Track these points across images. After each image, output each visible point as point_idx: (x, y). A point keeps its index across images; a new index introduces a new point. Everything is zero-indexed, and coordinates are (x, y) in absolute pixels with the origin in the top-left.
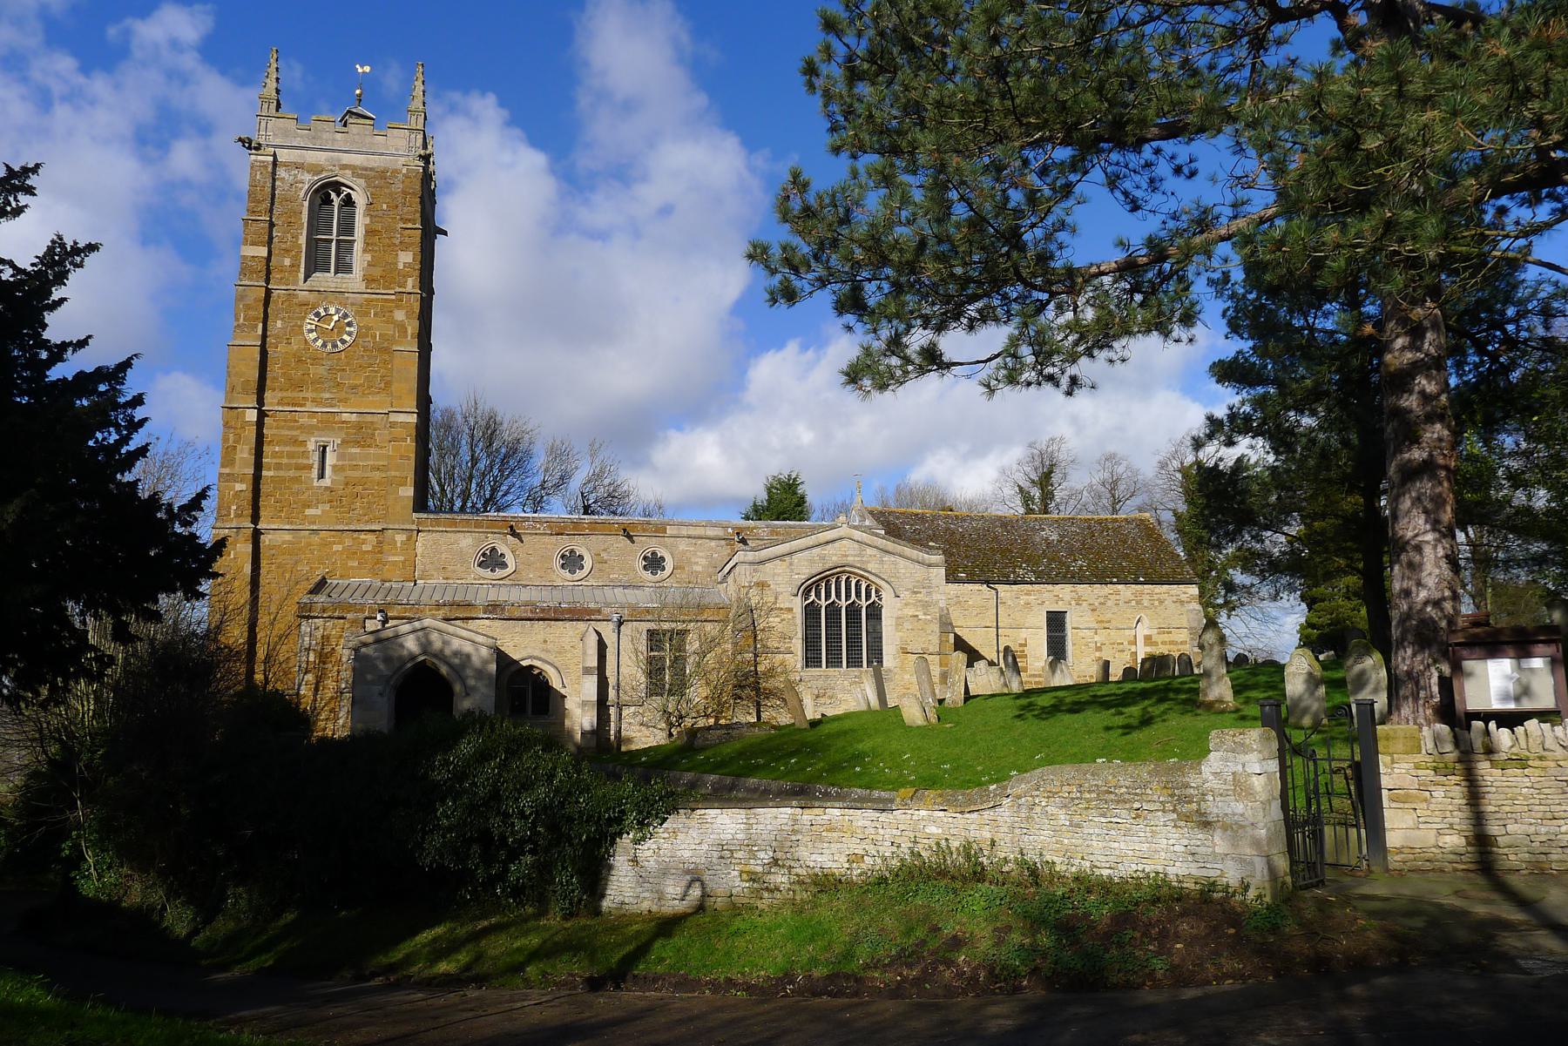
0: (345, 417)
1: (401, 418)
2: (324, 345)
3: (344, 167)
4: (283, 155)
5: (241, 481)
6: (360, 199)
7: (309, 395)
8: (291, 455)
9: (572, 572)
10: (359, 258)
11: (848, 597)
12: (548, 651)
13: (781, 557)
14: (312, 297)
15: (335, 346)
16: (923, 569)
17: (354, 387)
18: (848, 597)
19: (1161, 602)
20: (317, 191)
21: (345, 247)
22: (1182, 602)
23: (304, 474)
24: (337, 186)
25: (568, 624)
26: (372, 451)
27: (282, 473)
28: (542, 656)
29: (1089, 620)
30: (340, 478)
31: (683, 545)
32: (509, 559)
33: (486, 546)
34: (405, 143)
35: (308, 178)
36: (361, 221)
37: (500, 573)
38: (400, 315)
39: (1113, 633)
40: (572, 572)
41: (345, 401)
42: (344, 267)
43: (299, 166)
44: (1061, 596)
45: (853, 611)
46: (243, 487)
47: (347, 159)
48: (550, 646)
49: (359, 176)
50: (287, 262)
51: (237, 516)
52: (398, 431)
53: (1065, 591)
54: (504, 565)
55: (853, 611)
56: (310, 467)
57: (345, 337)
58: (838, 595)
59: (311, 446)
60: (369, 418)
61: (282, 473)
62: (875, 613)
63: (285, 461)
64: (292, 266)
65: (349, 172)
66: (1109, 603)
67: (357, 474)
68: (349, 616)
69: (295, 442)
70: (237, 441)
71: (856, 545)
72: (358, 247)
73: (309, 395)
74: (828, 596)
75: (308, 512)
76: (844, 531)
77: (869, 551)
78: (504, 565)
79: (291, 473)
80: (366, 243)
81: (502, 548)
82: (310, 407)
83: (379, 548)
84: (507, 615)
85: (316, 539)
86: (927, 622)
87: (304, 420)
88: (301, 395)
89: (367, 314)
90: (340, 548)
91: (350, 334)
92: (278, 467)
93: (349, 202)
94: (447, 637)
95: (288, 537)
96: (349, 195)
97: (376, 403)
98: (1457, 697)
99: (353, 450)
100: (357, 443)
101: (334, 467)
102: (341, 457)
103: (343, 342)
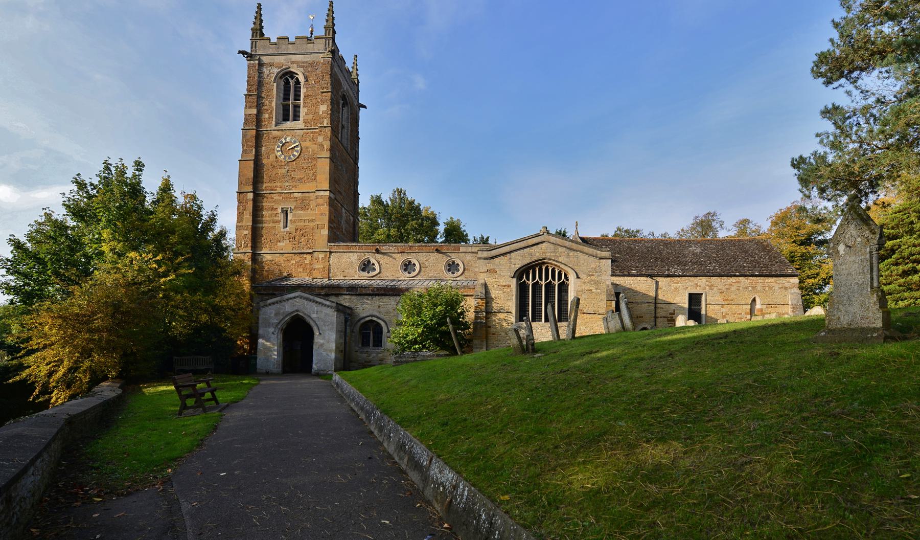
0: (296, 195)
1: (322, 193)
2: (285, 158)
3: (293, 63)
4: (265, 59)
6: (301, 78)
7: (279, 184)
10: (303, 111)
11: (547, 278)
13: (504, 254)
16: (597, 260)
18: (547, 278)
19: (770, 288)
20: (281, 78)
21: (297, 108)
22: (786, 288)
23: (276, 225)
26: (309, 212)
28: (377, 314)
29: (719, 299)
30: (294, 226)
31: (469, 257)
34: (323, 46)
35: (276, 71)
38: (320, 139)
39: (734, 307)
42: (296, 118)
43: (271, 65)
44: (699, 284)
45: (549, 286)
46: (247, 232)
48: (382, 310)
49: (301, 67)
52: (320, 201)
53: (702, 281)
54: (374, 269)
55: (549, 286)
56: (279, 221)
57: (295, 153)
58: (541, 278)
59: (280, 211)
60: (307, 195)
62: (563, 288)
65: (295, 65)
66: (733, 289)
67: (302, 224)
71: (552, 246)
73: (279, 184)
74: (534, 278)
75: (279, 244)
77: (560, 249)
79: (271, 225)
81: (373, 261)
82: (279, 190)
86: (597, 294)
90: (293, 262)
93: (298, 82)
94: (366, 308)
97: (309, 187)
102: (294, 216)
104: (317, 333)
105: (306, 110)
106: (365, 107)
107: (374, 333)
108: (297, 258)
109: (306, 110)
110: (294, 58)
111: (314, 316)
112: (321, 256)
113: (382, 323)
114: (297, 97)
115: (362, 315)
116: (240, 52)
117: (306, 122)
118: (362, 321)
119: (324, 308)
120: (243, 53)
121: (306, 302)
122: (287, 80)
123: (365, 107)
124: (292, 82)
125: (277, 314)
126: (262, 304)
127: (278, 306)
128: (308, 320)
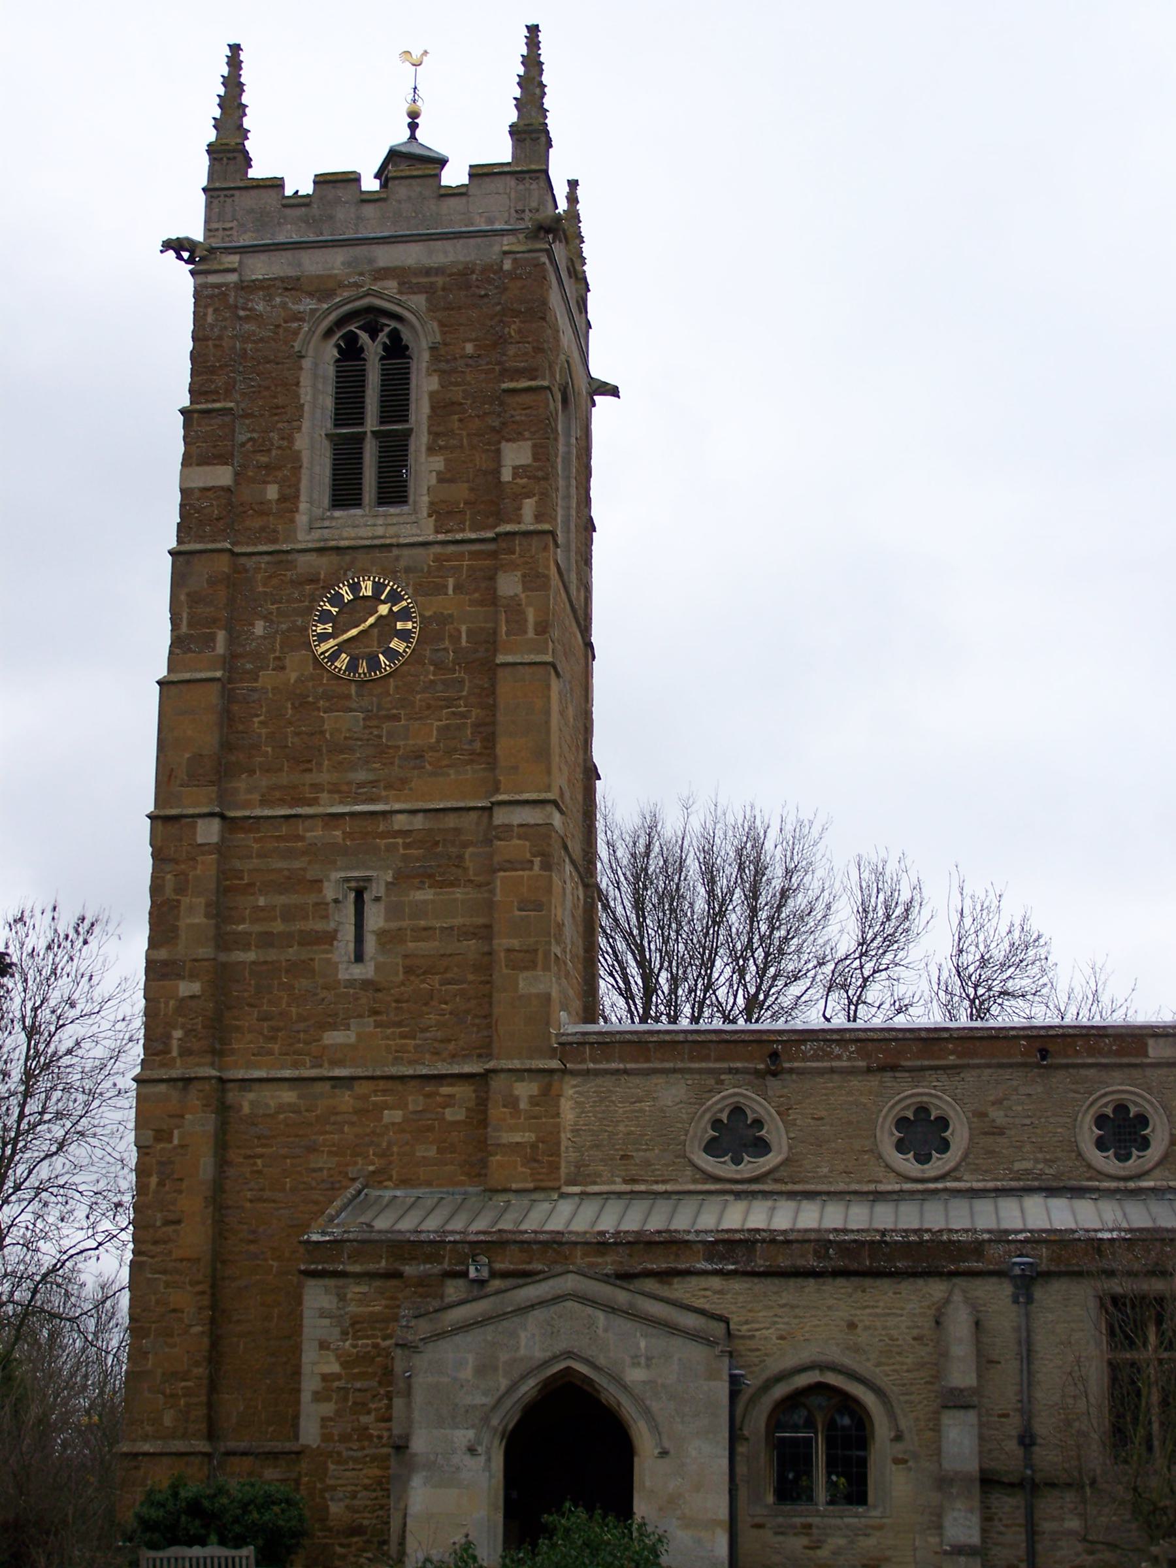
0: (400, 822)
3: (383, 274)
5: (193, 977)
6: (422, 341)
8: (288, 914)
9: (923, 1159)
10: (425, 468)
12: (856, 1349)
13: (362, 538)
14: (323, 565)
15: (374, 665)
17: (418, 755)
21: (395, 452)
24: (372, 318)
25: (906, 1286)
27: (272, 955)
28: (847, 1361)
32: (776, 1133)
33: (719, 1102)
36: (424, 385)
37: (751, 1166)
40: (923, 1159)
41: (398, 785)
42: (393, 491)
43: (292, 286)
46: (195, 988)
47: (386, 256)
50: (272, 492)
51: (185, 1052)
54: (762, 1147)
56: (330, 938)
57: (396, 644)
60: (451, 821)
61: (272, 955)
63: (278, 927)
64: (283, 499)
67: (424, 947)
68: (408, 1270)
69: (293, 882)
70: (181, 890)
72: (420, 441)
73: (325, 777)
75: (334, 1038)
76: (570, 1283)
78: (762, 1147)
79: (292, 953)
80: (434, 435)
83: (480, 1116)
84: (760, 1264)
85: (346, 1100)
87: (316, 834)
88: (308, 778)
89: (441, 589)
91: (404, 635)
92: (267, 940)
93: (397, 349)
95: (288, 1096)
96: (395, 335)
98: (1124, 1031)
99: (420, 896)
100: (426, 877)
101: (381, 934)
102: (394, 911)
103: (392, 654)
104: (645, 1442)
105: (438, 463)
106: (614, 392)
107: (830, 1443)
108: (415, 1101)
109: (438, 463)
110: (386, 256)
111: (635, 1375)
112: (525, 1090)
113: (868, 1399)
114: (396, 404)
115: (775, 1366)
116: (168, 245)
117: (442, 513)
118: (780, 1391)
119: (677, 1342)
120: (175, 246)
121: (601, 1317)
122: (351, 338)
123: (614, 392)
124: (373, 349)
125: (482, 1370)
126: (424, 1327)
127: (489, 1333)
128: (611, 1393)
